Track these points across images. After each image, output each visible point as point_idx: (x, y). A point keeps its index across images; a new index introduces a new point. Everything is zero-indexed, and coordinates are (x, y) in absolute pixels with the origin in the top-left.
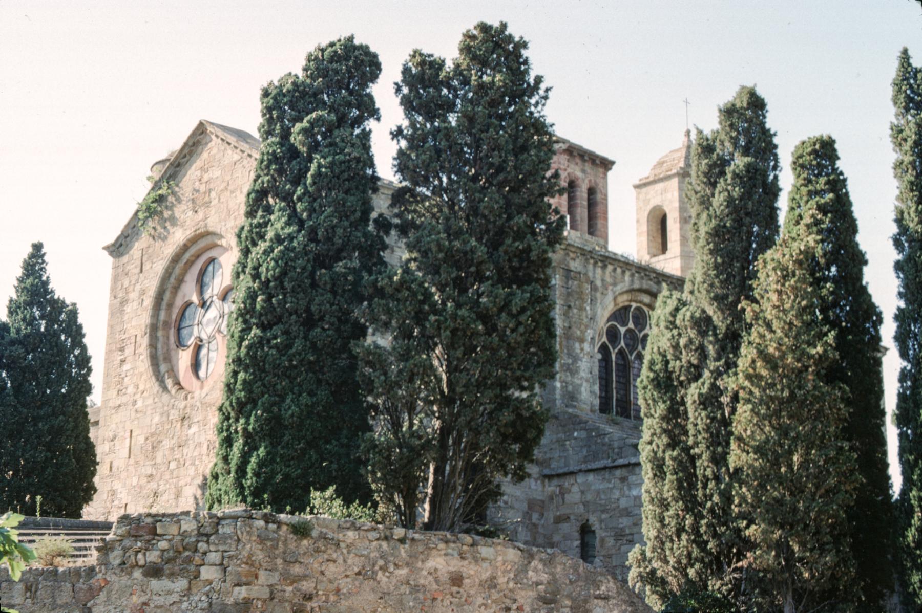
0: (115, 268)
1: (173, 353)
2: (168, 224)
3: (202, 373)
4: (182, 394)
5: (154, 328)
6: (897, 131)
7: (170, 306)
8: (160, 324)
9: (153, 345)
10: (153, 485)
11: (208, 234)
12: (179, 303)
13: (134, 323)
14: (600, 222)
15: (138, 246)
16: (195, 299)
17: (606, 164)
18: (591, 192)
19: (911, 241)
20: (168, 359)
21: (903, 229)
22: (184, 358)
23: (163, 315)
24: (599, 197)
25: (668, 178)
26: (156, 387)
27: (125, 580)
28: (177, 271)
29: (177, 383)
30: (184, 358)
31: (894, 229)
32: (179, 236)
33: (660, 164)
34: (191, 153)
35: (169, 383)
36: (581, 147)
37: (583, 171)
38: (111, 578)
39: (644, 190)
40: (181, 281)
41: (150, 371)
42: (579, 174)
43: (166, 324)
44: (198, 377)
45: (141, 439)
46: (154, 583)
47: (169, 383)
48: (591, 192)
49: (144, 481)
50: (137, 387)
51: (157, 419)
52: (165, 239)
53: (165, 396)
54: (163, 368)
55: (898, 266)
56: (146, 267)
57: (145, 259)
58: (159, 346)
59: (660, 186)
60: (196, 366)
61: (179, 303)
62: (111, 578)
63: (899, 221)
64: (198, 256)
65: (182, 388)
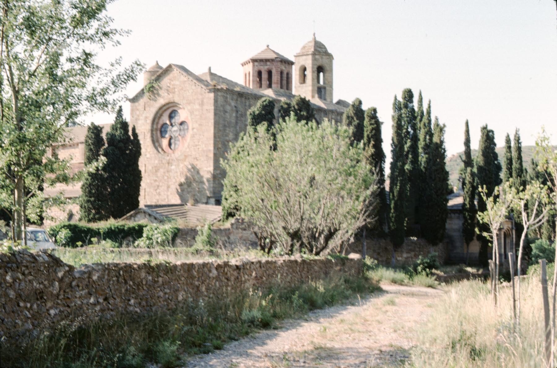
0: (132, 106)
1: (160, 139)
2: (156, 96)
3: (173, 146)
4: (166, 155)
5: (152, 131)
6: (393, 117)
7: (158, 123)
8: (154, 129)
9: (152, 136)
10: (157, 183)
11: (174, 102)
12: (161, 122)
13: (143, 127)
14: (290, 85)
15: (142, 101)
16: (168, 122)
17: (292, 63)
18: (288, 74)
19: (395, 146)
20: (158, 141)
21: (393, 142)
22: (165, 142)
23: (155, 126)
24: (290, 76)
25: (307, 55)
26: (155, 151)
27: (237, 231)
28: (160, 112)
29: (163, 150)
30: (165, 142)
31: (391, 142)
32: (161, 101)
33: (304, 47)
34: (165, 73)
35: (160, 150)
36: (283, 56)
37: (285, 67)
38: (234, 230)
39: (298, 58)
40: (161, 115)
41: (152, 145)
42: (284, 68)
43: (157, 130)
44: (171, 148)
45: (150, 168)
46: (244, 232)
47: (160, 150)
48: (288, 74)
49: (153, 182)
50: (146, 150)
51: (157, 162)
52: (155, 101)
53: (160, 155)
54: (157, 144)
55: (392, 151)
56: (147, 109)
57: (146, 106)
58: (154, 137)
59: (304, 57)
60: (170, 144)
61: (161, 122)
62: (234, 230)
63: (393, 140)
64: (168, 108)
65: (165, 152)
